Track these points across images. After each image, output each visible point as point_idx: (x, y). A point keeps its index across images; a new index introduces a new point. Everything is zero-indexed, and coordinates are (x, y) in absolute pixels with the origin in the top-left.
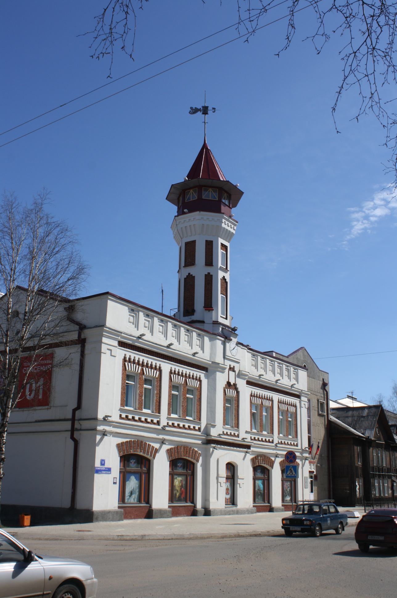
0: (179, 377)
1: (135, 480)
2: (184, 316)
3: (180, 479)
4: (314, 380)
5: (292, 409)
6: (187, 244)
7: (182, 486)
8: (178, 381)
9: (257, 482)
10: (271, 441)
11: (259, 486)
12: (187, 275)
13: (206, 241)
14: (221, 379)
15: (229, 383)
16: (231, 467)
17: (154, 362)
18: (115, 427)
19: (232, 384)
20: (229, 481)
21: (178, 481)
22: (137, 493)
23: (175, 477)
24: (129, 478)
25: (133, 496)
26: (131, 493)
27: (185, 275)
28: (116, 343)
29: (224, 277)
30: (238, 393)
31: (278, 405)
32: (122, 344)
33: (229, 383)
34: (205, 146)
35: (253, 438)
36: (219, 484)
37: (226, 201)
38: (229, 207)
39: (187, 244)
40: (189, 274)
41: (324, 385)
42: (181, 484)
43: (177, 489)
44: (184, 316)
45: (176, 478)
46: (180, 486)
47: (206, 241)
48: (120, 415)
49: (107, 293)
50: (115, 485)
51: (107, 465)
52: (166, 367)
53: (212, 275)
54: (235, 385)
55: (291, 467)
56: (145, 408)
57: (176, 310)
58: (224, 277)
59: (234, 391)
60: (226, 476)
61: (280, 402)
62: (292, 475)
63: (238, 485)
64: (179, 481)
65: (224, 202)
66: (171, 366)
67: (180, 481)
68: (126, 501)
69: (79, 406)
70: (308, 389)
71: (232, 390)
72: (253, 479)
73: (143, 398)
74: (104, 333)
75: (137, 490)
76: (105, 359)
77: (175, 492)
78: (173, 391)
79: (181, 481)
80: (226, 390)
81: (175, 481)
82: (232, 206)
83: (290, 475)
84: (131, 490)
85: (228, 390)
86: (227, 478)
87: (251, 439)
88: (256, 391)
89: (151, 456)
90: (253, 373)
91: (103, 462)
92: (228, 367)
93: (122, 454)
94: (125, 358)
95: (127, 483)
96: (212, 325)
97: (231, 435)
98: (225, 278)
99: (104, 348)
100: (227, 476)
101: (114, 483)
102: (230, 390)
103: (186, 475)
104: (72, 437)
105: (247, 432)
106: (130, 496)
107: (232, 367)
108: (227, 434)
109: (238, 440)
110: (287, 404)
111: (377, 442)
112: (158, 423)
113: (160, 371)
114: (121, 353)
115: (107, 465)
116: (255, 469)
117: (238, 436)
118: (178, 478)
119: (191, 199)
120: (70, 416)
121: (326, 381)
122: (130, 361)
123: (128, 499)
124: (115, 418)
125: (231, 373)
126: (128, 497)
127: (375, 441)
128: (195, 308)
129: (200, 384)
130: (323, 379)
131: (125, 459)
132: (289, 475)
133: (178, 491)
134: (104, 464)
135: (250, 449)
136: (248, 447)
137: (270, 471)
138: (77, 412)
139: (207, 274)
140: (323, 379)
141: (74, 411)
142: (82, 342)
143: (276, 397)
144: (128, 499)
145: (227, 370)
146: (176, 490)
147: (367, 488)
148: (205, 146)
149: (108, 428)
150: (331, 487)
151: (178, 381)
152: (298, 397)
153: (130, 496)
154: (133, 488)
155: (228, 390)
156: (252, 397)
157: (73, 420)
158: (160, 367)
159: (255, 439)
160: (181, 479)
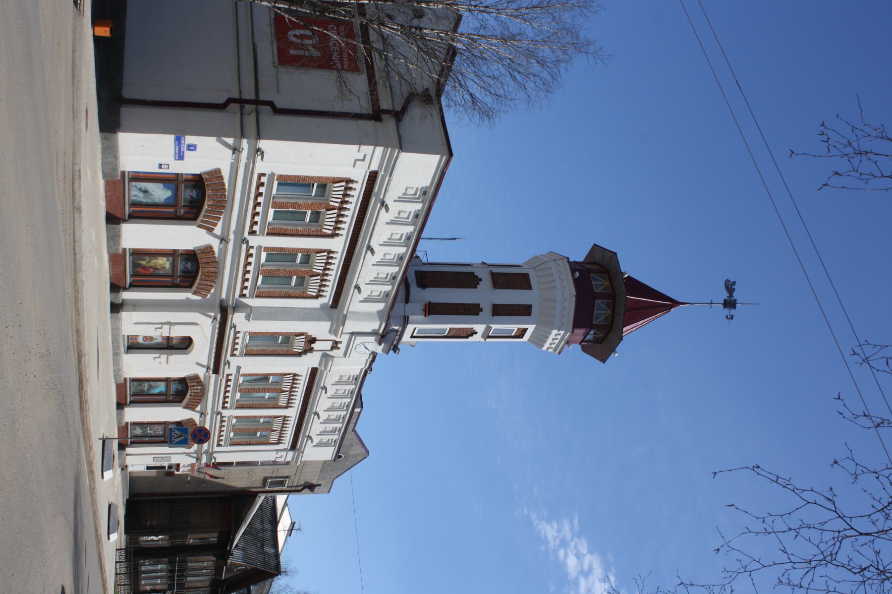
0: (323, 265)
1: (166, 197)
2: (417, 272)
3: (168, 265)
4: (319, 470)
5: (274, 437)
6: (526, 276)
7: (156, 269)
8: (328, 218)
9: (163, 384)
10: (226, 405)
11: (156, 387)
12: (479, 277)
13: (530, 306)
14: (320, 329)
15: (313, 340)
16: (186, 344)
17: (328, 289)
18: (247, 166)
19: (313, 345)
20: (164, 341)
21: (163, 263)
22: (145, 201)
23: (171, 259)
24: (168, 188)
25: (141, 195)
26: (145, 192)
27: (479, 273)
28: (374, 167)
29: (476, 333)
30: (299, 354)
31: (281, 416)
32: (373, 177)
33: (313, 340)
34: (676, 303)
35: (230, 377)
36: (159, 326)
37: (592, 336)
38: (583, 341)
39: (526, 276)
40: (481, 280)
41: (311, 487)
42: (159, 267)
43: (152, 262)
44: (417, 272)
45: (168, 260)
46: (156, 267)
47: (530, 306)
48: (264, 175)
49: (451, 154)
50: (158, 166)
51: (188, 154)
52: (338, 245)
53: (478, 315)
54: (311, 350)
55: (186, 436)
56: (275, 212)
57: (424, 260)
58: (476, 333)
59: (302, 348)
60: (171, 336)
61: (285, 418)
62: (173, 438)
63: (158, 355)
64: (163, 264)
65: (590, 333)
66: (340, 251)
67: (165, 266)
68: (133, 183)
69: (278, 111)
70: (305, 461)
71: (303, 345)
72: (168, 378)
73: (290, 209)
74: (390, 149)
75: (149, 201)
76: (350, 151)
77: (147, 258)
78: (302, 255)
79: (164, 268)
80: (304, 337)
81: (165, 259)
82: (583, 345)
83: (173, 434)
84: (150, 190)
85: (304, 340)
86: (168, 337)
87: (228, 375)
88: (302, 382)
89: (202, 221)
90: (329, 379)
91: (192, 147)
92: (338, 340)
93: (205, 177)
94: (352, 181)
95: (161, 185)
96: (403, 315)
97: (235, 344)
98: (474, 335)
99: (367, 149)
100: (172, 337)
101: (160, 165)
102: (303, 343)
103: (173, 276)
104: (230, 101)
105: (239, 368)
106: (140, 190)
107: (339, 345)
108: (236, 338)
109: (227, 355)
110: (282, 430)
111: (225, 567)
112: (252, 233)
113: (287, 407)
114: (360, 175)
115: (188, 154)
116: (182, 381)
117: (233, 355)
118: (168, 263)
119: (595, 283)
120: (263, 97)
121: (317, 489)
122: (347, 189)
123: (136, 187)
124: (261, 166)
125: (330, 344)
126: (139, 187)
127: (226, 564)
128: (428, 289)
129: (312, 297)
130: (320, 485)
131: (198, 182)
132: (173, 433)
133: (148, 263)
134: (189, 149)
135: (213, 373)
136: (216, 371)
137: (189, 289)
138: (268, 109)
139: (481, 307)
140: (320, 485)
141: (271, 104)
142: (376, 115)
143: (293, 413)
144: (136, 187)
145: (333, 338)
146: (150, 260)
147: (154, 553)
148: (676, 303)
149: (244, 155)
150: (156, 498)
151: (328, 218)
152: (293, 447)
153: (140, 190)
154: (152, 193)
155: (304, 340)
156: (292, 375)
157: (257, 102)
158: (337, 235)
159: (228, 380)
160: (167, 268)
